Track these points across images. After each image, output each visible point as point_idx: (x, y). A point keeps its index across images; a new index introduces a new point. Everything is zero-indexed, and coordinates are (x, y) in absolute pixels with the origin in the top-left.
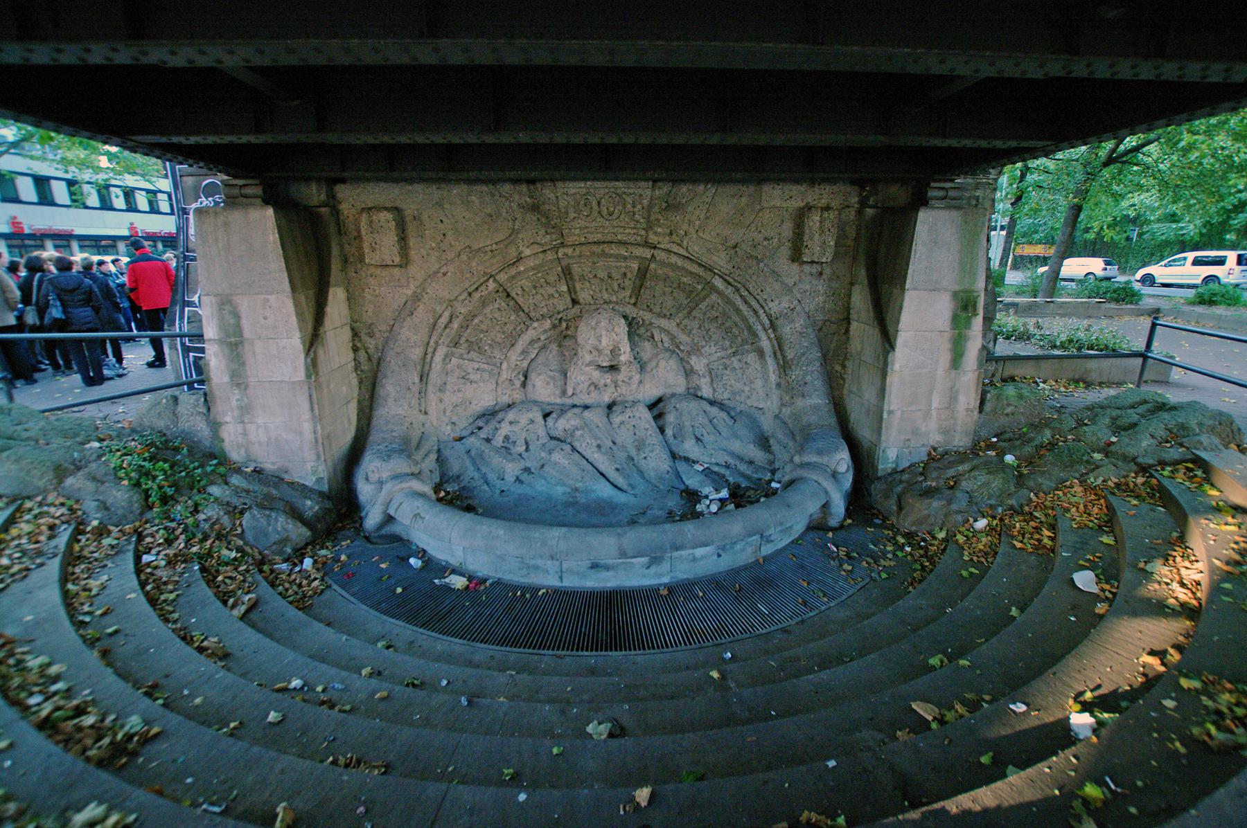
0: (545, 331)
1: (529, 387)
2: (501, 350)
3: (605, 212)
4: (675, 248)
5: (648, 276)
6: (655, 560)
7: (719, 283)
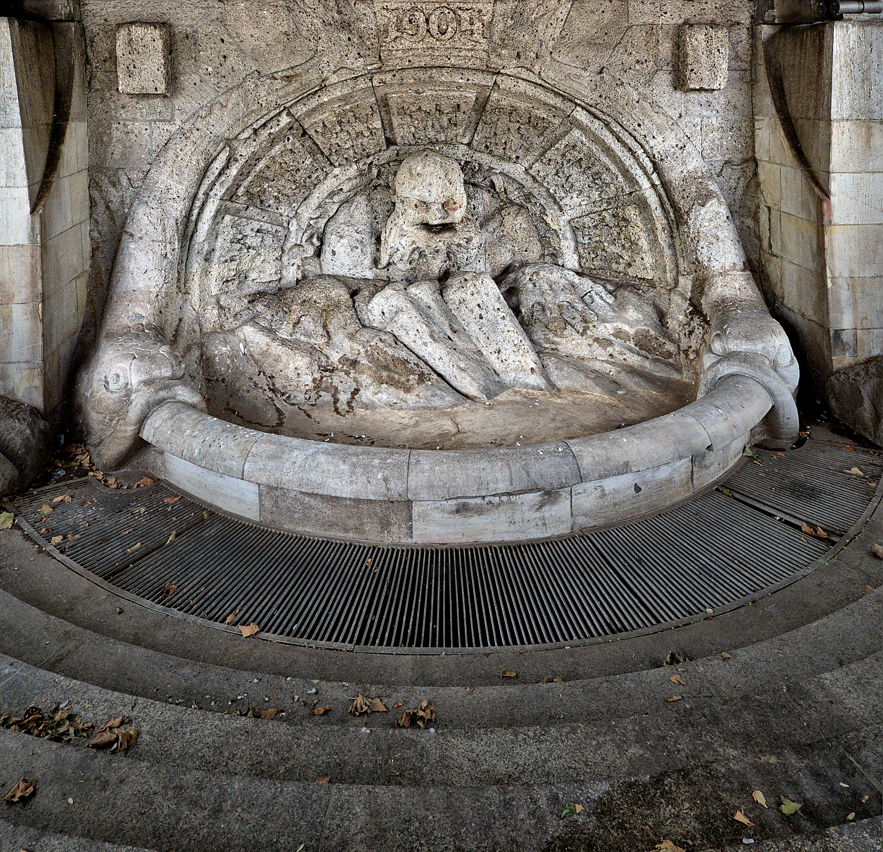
0: (349, 179)
1: (327, 255)
2: (290, 204)
3: (434, 28)
4: (525, 74)
5: (488, 107)
6: (550, 495)
7: (581, 116)
